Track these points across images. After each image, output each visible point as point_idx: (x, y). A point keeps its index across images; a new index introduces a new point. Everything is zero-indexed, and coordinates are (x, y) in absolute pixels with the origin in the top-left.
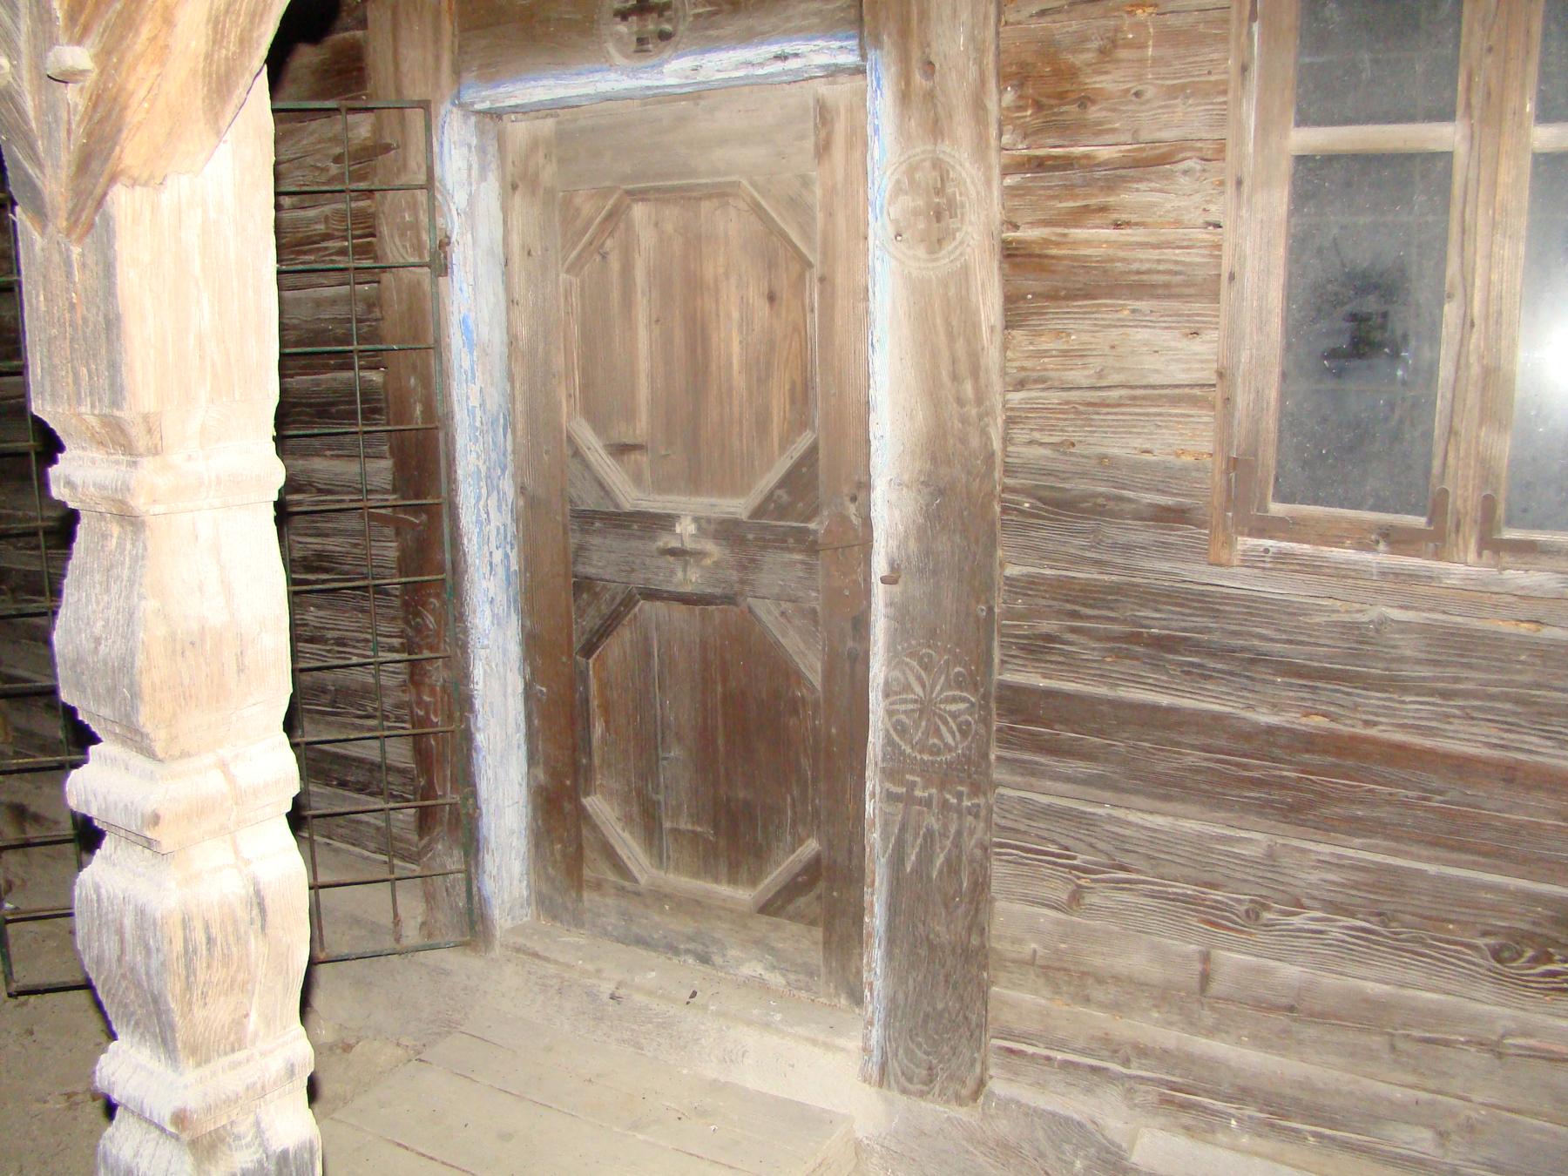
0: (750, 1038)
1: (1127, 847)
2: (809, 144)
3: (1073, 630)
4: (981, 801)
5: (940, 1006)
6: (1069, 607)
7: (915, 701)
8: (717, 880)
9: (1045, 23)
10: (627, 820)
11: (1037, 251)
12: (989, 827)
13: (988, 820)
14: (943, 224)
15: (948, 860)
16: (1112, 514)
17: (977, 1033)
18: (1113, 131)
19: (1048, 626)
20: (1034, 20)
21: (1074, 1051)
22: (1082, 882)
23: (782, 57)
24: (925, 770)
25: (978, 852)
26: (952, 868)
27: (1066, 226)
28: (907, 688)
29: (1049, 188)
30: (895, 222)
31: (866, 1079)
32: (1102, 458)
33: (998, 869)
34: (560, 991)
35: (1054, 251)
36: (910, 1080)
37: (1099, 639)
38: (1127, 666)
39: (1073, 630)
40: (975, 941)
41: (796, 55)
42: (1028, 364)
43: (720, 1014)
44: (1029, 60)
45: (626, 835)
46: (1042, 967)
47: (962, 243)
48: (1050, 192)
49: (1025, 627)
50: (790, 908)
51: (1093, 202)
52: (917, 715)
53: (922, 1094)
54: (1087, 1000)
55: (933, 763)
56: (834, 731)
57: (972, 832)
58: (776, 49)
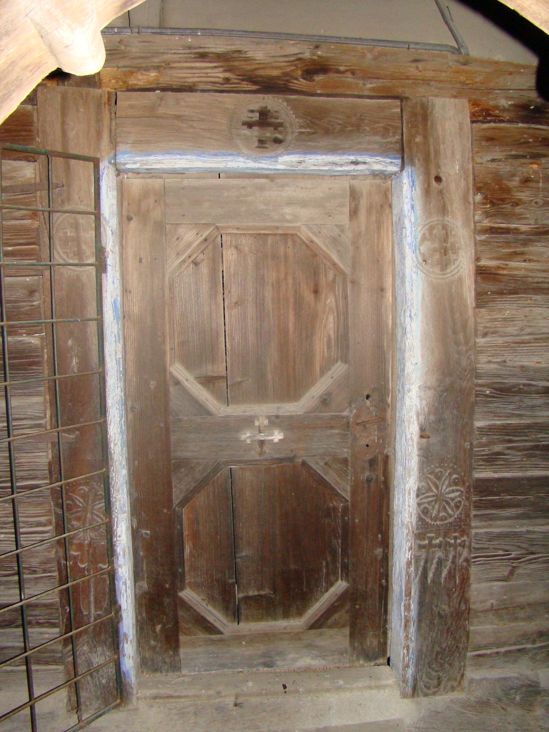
0: (333, 698)
1: (535, 543)
2: (346, 210)
3: (509, 448)
4: (465, 538)
5: (444, 646)
6: (507, 438)
7: (433, 496)
8: (275, 618)
9: (494, 165)
10: (211, 599)
11: (494, 272)
12: (470, 552)
13: (470, 547)
14: (447, 256)
15: (449, 572)
16: (527, 392)
17: (463, 653)
18: (527, 218)
19: (497, 448)
20: (490, 163)
21: (510, 645)
22: (514, 565)
23: (356, 163)
24: (437, 530)
25: (465, 564)
26: (451, 576)
27: (506, 261)
28: (430, 490)
29: (499, 242)
30: (423, 255)
31: (404, 695)
32: (523, 367)
33: (473, 570)
34: (195, 714)
35: (501, 272)
36: (428, 688)
37: (520, 451)
38: (534, 461)
39: (509, 448)
40: (463, 607)
41: (365, 163)
42: (488, 325)
43: (309, 691)
44: (489, 182)
45: (210, 608)
46: (495, 610)
47: (458, 266)
48: (499, 244)
49: (486, 451)
50: (330, 622)
51: (517, 250)
52: (433, 503)
53: (434, 693)
54: (516, 619)
55: (442, 525)
56: (357, 521)
57: (460, 555)
58: (352, 158)
